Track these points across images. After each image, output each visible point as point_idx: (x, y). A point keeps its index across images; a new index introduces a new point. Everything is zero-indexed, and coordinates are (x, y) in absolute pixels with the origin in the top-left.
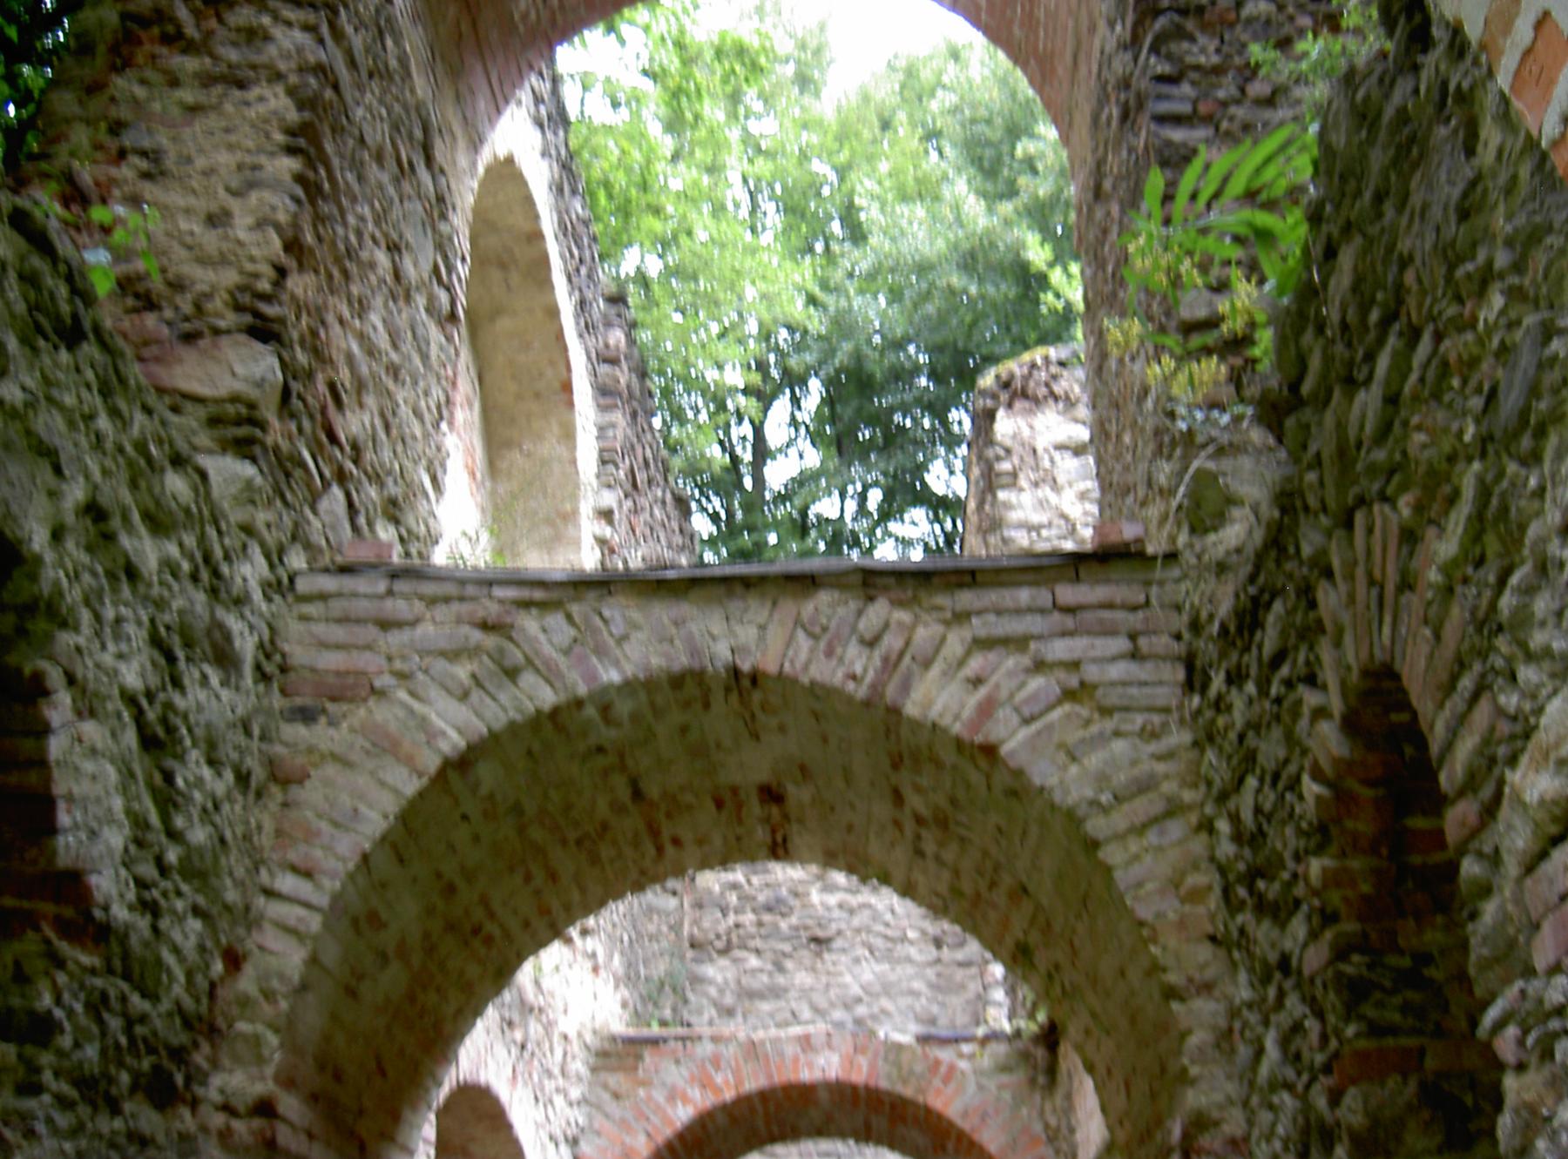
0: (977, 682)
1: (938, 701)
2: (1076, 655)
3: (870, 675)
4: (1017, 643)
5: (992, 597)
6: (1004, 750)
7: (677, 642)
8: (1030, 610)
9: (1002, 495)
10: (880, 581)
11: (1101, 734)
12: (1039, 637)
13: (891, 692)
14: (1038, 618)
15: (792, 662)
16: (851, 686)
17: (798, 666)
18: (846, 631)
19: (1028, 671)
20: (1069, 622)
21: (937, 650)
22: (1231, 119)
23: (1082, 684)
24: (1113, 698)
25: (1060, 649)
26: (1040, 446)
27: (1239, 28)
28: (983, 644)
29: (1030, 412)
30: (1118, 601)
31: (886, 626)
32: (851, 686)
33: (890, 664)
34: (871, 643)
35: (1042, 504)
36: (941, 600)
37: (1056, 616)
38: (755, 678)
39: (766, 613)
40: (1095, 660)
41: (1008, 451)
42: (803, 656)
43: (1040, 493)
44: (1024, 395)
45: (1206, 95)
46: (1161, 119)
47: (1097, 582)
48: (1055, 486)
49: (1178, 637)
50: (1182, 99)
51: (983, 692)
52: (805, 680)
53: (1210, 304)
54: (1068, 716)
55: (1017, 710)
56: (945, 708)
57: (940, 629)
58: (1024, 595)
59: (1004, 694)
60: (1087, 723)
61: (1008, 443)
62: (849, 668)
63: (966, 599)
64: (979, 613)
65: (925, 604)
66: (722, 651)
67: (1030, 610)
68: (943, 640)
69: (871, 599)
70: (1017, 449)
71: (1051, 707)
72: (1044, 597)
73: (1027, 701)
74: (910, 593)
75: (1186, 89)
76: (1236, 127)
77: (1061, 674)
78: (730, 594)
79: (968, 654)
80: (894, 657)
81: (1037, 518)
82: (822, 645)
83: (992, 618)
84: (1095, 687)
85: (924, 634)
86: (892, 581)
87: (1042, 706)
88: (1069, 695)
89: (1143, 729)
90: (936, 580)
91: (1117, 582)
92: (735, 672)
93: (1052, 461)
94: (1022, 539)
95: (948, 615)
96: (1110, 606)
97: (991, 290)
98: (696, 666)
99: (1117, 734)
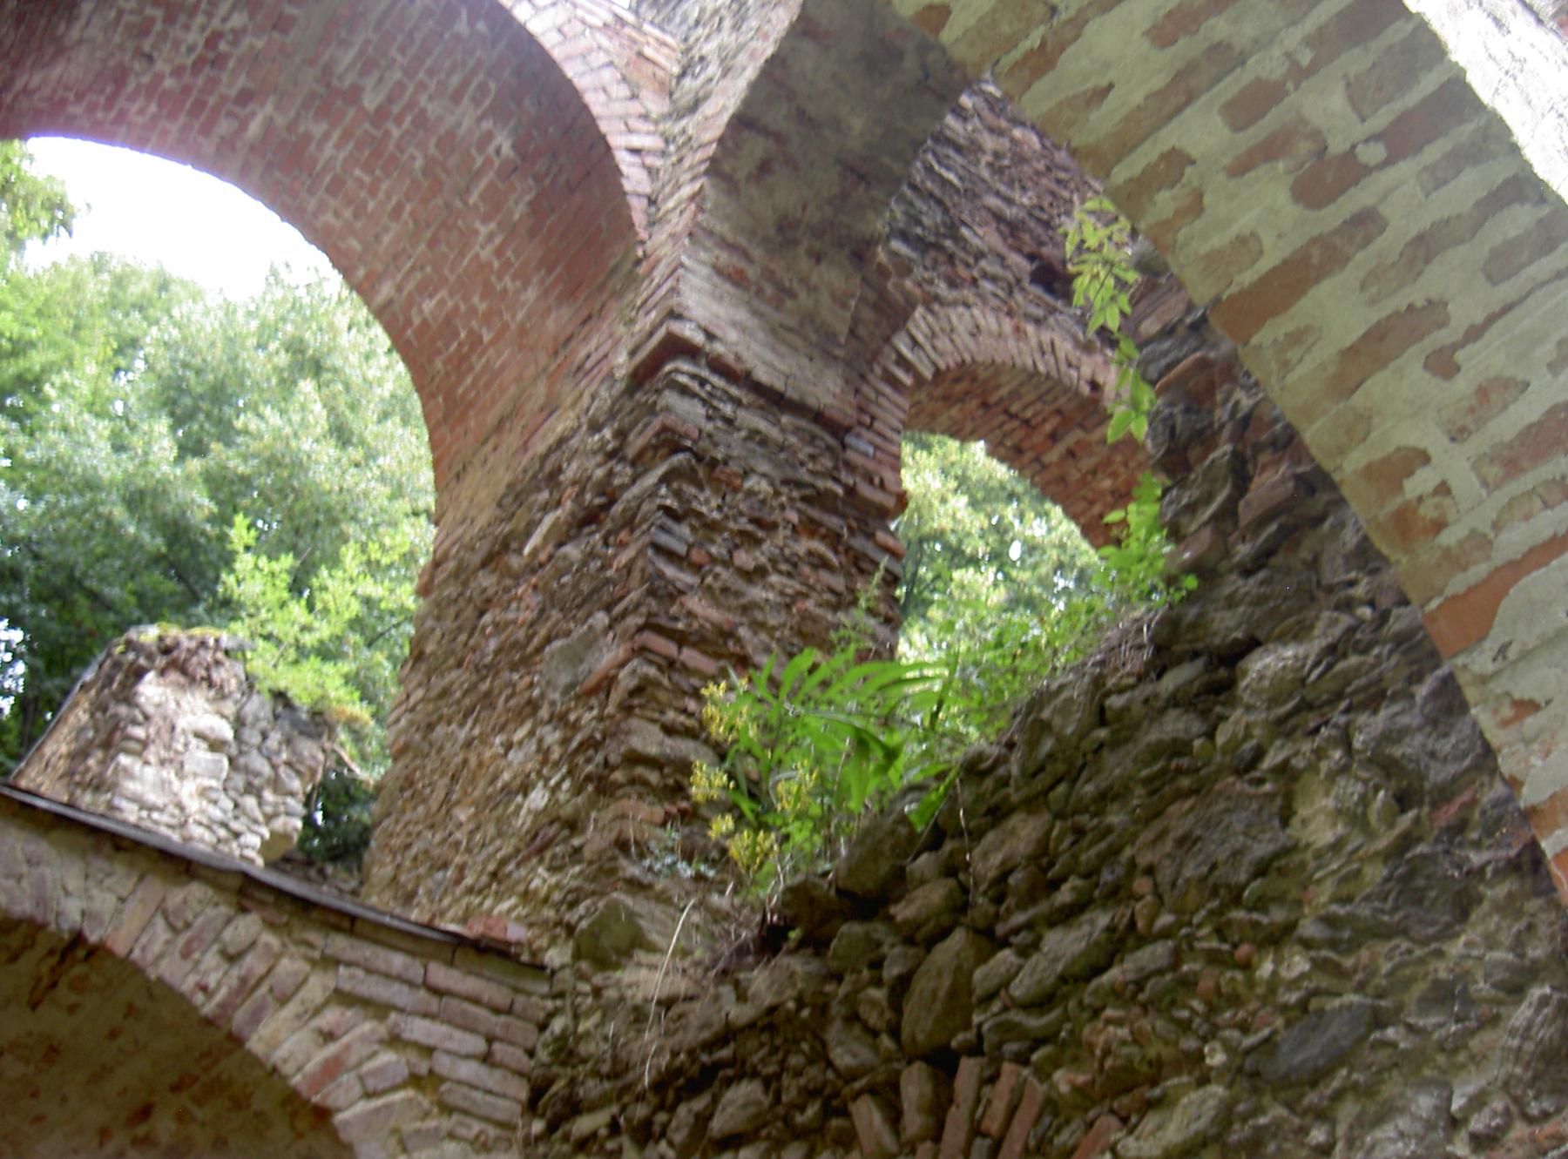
0: (329, 1036)
1: (286, 1042)
2: (431, 1041)
3: (223, 992)
4: (379, 1009)
5: (366, 951)
6: (339, 1118)
7: (25, 883)
8: (400, 979)
9: (124, 760)
10: (260, 895)
11: (437, 1129)
12: (401, 1011)
13: (239, 1017)
14: (405, 989)
15: (144, 949)
16: (199, 998)
17: (150, 957)
18: (209, 936)
19: (381, 1042)
20: (434, 1004)
21: (298, 988)
22: (716, 576)
23: (431, 1072)
24: (455, 1099)
25: (418, 1029)
26: (181, 723)
27: (740, 496)
28: (343, 998)
29: (182, 687)
30: (485, 998)
31: (253, 944)
32: (199, 998)
33: (246, 987)
34: (232, 958)
35: (164, 785)
36: (313, 936)
37: (423, 993)
38: (97, 952)
39: (130, 884)
40: (448, 1052)
41: (147, 718)
42: (157, 948)
43: (164, 773)
44: (184, 671)
45: (701, 545)
46: (659, 549)
47: (470, 973)
48: (181, 774)
49: (531, 1053)
50: (680, 539)
51: (332, 1049)
52: (152, 974)
53: (661, 744)
54: (410, 1100)
55: (361, 1079)
56: (291, 1054)
57: (305, 967)
58: (398, 961)
59: (353, 1059)
60: (426, 1115)
61: (150, 710)
62: (202, 977)
63: (340, 944)
64: (349, 964)
65: (296, 935)
66: (72, 911)
67: (400, 979)
68: (305, 980)
69: (244, 910)
70: (158, 720)
71: (394, 1088)
72: (416, 970)
73: (373, 1073)
74: (285, 918)
75: (684, 530)
76: (717, 585)
77: (413, 1056)
78: (97, 849)
79: (326, 1004)
80: (252, 982)
81: (152, 798)
82: (181, 940)
83: (360, 973)
84: (442, 1079)
85: (291, 966)
86: (270, 899)
87: (387, 1084)
88: (415, 1080)
89: (477, 1137)
90: (315, 915)
91: (489, 979)
92: (78, 938)
93: (186, 745)
94: (131, 813)
95: (316, 954)
96: (476, 1001)
97: (146, 537)
98: (39, 918)
99: (452, 1136)
